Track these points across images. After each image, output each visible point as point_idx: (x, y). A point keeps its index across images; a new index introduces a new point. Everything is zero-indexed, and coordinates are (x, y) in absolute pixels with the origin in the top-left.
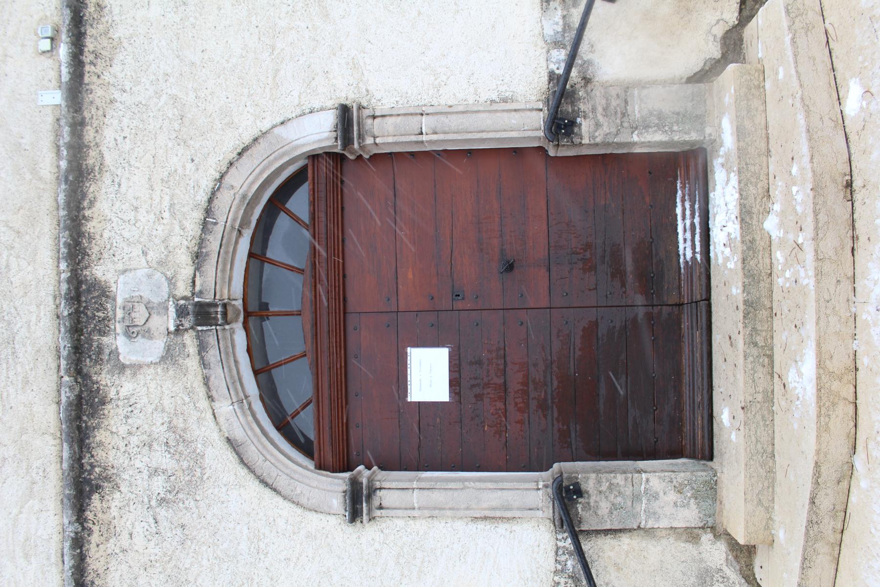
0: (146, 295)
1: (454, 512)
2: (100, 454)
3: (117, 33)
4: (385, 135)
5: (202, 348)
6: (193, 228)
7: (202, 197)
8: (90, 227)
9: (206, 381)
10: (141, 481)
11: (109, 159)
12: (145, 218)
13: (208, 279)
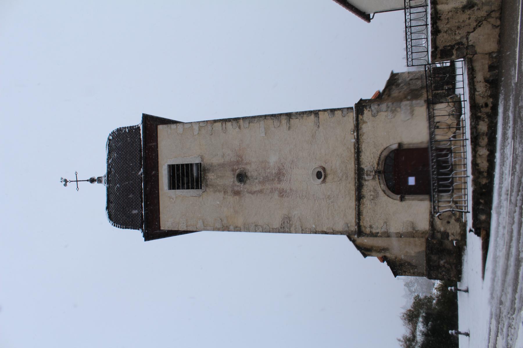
7: (378, 156)
8: (361, 160)
12: (369, 159)
13: (399, 199)
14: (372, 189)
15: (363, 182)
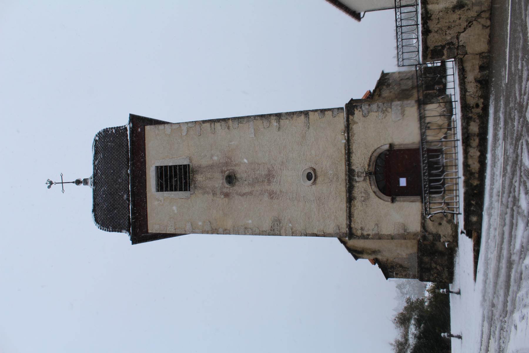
0: (361, 170)
1: (407, 201)
2: (353, 195)
3: (355, 132)
4: (396, 148)
5: (370, 179)
6: (368, 161)
7: (369, 157)
9: (370, 183)
10: (360, 198)
11: (354, 151)
14: (363, 190)
15: (354, 183)
